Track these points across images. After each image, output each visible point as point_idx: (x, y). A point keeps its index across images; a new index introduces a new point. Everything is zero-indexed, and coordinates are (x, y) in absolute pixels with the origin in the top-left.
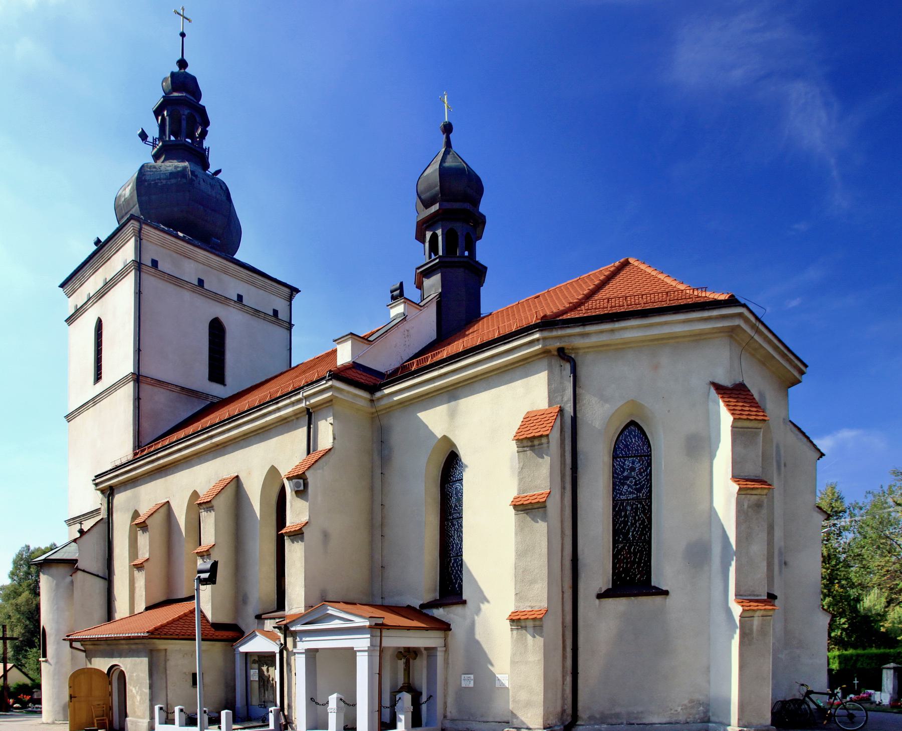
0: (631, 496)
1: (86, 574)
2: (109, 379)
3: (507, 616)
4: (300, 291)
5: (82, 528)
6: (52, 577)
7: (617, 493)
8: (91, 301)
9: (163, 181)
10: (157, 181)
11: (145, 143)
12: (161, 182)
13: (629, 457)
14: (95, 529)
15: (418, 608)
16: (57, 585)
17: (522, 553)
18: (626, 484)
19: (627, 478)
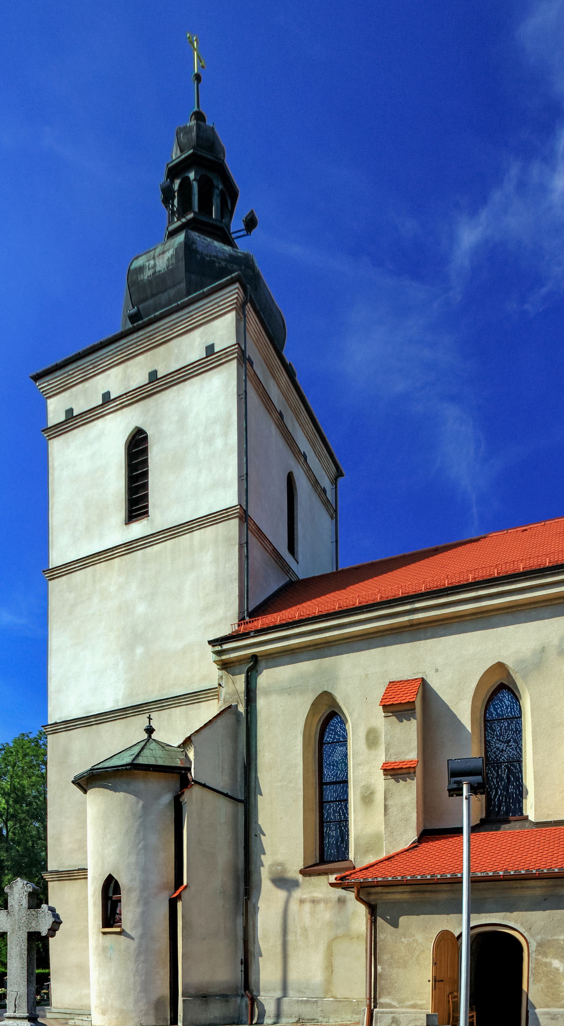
1: (206, 790)
3: (380, 767)
6: (135, 795)
8: (118, 403)
9: (221, 262)
10: (213, 258)
12: (219, 263)
14: (219, 721)
16: (145, 808)
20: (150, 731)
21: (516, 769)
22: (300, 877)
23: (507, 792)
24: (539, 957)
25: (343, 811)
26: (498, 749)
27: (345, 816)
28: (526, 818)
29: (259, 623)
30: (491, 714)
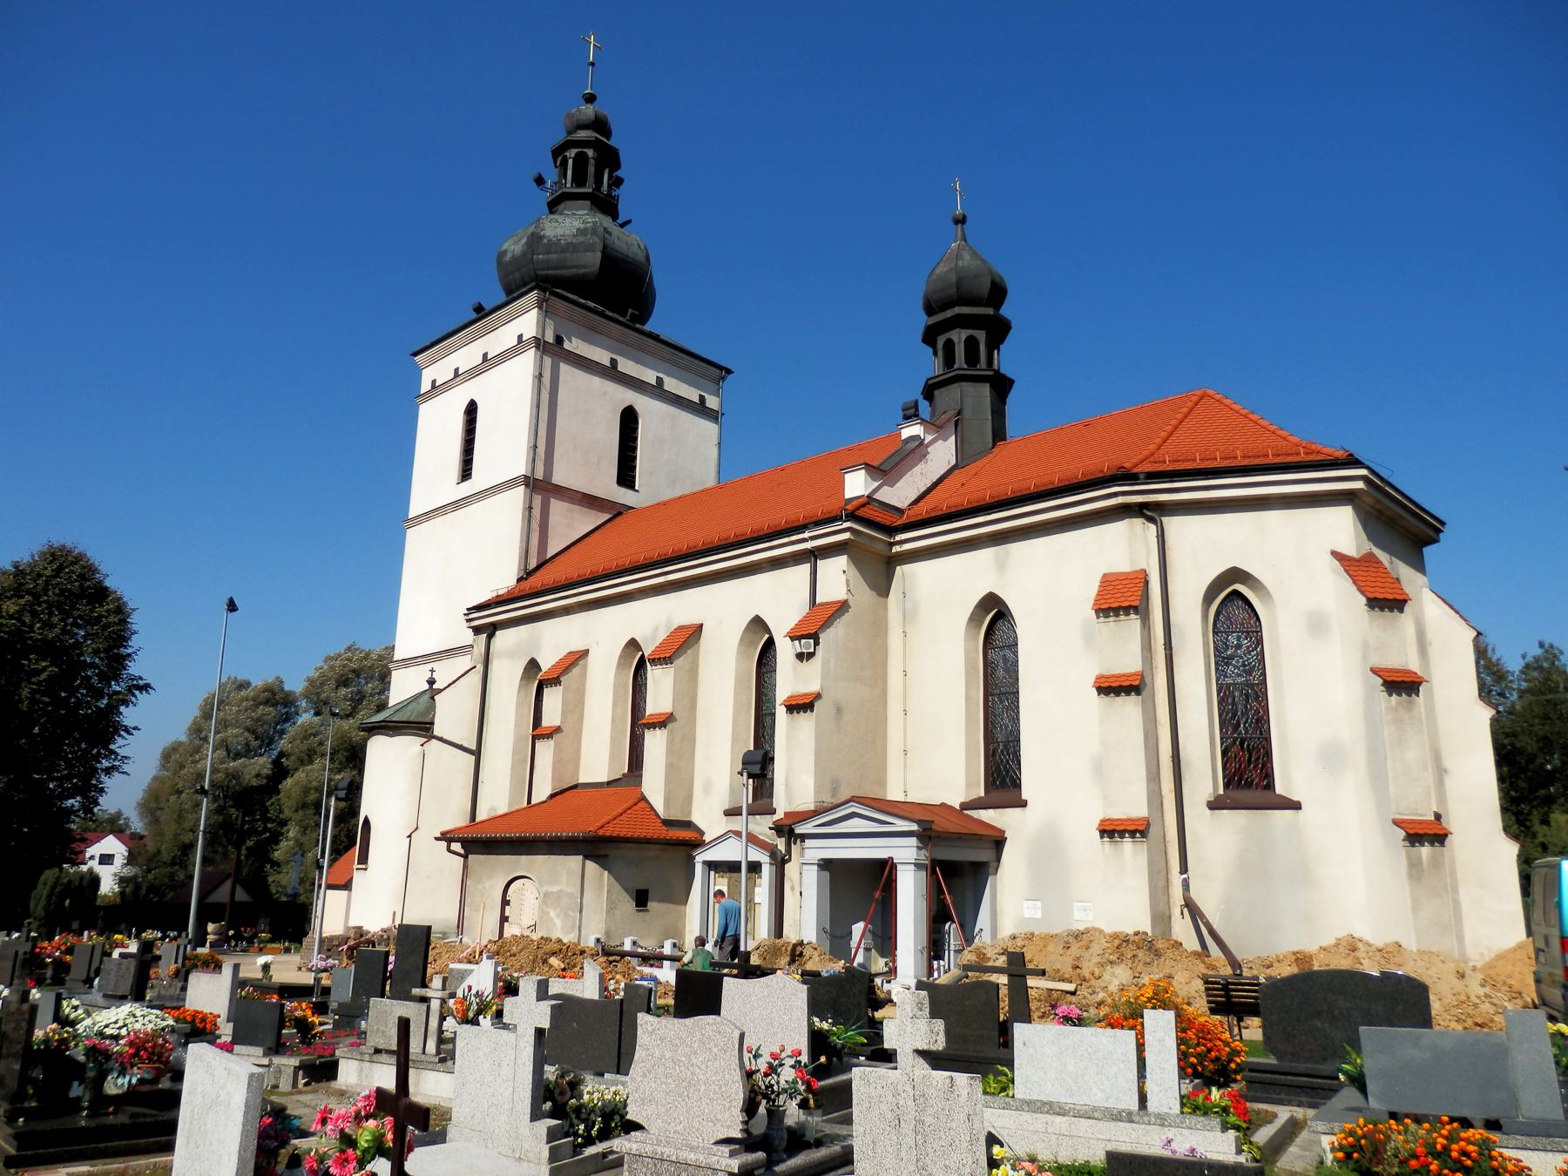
0: (1240, 680)
2: (483, 474)
4: (733, 372)
5: (434, 676)
7: (1220, 675)
11: (541, 189)
13: (1233, 632)
15: (958, 808)
17: (525, 494)
18: (1231, 664)
19: (1232, 657)
29: (527, 585)
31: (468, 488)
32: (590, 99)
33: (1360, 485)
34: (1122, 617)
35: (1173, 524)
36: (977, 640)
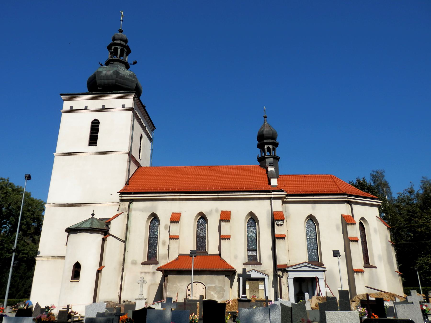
20: (93, 215)
21: (204, 238)
22: (363, 269)
23: (202, 244)
24: (208, 291)
25: (155, 246)
26: (200, 233)
27: (156, 247)
28: (207, 253)
30: (199, 223)
31: (92, 149)
32: (121, 31)
33: (381, 204)
34: (352, 225)
35: (354, 206)
36: (195, 222)
